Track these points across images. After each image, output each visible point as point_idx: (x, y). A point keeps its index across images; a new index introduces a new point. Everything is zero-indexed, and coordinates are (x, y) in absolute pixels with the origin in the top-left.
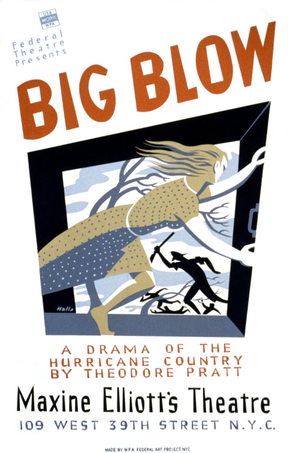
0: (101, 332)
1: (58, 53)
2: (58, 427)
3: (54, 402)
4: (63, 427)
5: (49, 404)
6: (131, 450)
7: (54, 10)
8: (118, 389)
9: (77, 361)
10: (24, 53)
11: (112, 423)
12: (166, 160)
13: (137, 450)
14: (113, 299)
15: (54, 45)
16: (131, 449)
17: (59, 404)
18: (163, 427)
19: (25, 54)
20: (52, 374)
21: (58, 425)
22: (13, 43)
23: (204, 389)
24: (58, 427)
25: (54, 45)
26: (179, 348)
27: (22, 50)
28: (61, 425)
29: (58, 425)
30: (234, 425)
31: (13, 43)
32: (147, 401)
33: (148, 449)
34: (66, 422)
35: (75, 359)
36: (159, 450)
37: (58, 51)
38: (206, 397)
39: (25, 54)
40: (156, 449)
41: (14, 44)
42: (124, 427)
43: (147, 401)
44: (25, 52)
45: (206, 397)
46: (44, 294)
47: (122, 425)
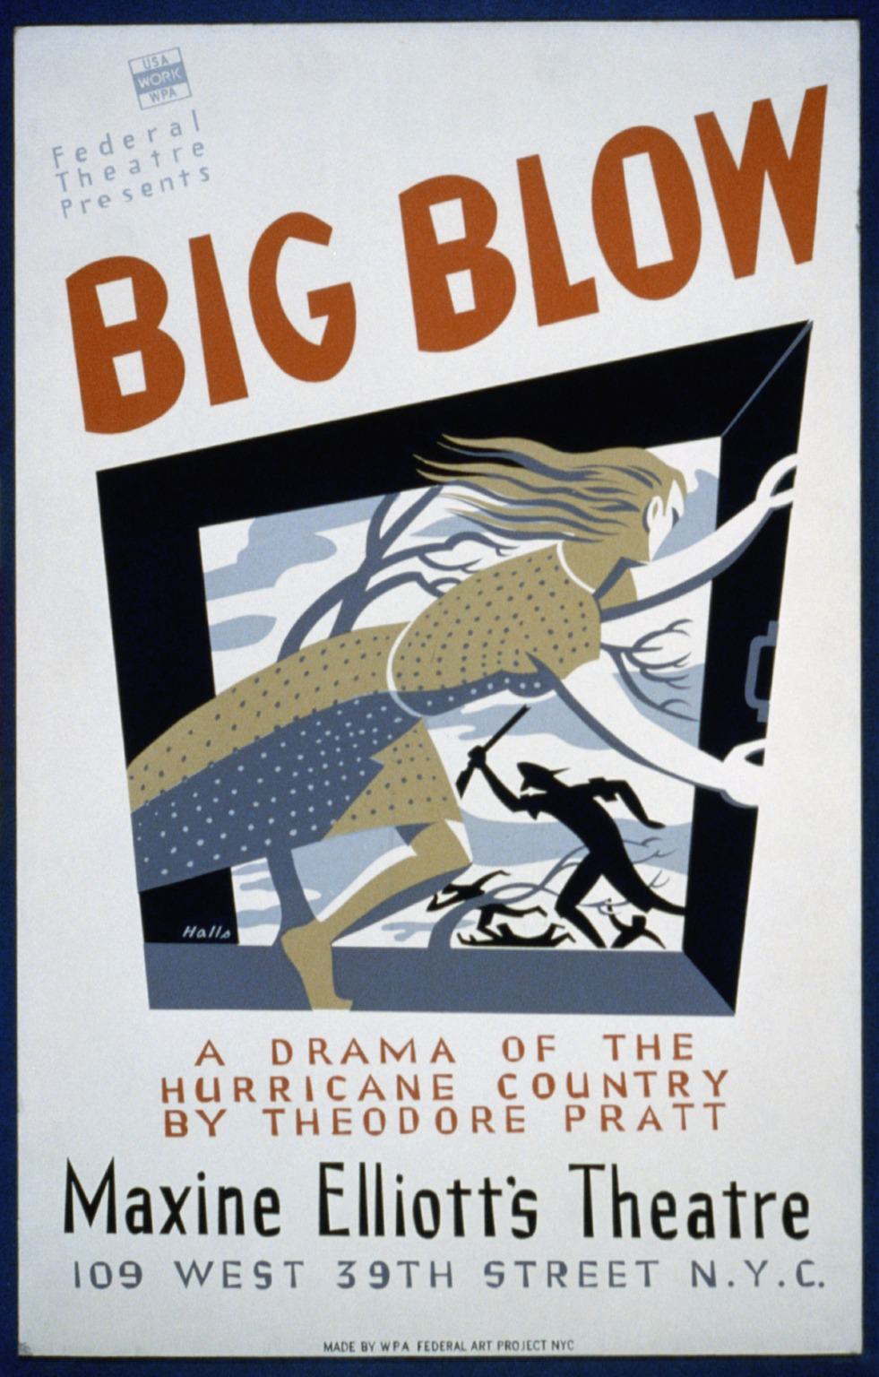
2: (186, 1281)
3: (175, 1207)
21: (186, 1273)
24: (186, 1281)
26: (541, 1048)
29: (186, 1273)
32: (447, 1203)
41: (58, 151)
43: (447, 1203)
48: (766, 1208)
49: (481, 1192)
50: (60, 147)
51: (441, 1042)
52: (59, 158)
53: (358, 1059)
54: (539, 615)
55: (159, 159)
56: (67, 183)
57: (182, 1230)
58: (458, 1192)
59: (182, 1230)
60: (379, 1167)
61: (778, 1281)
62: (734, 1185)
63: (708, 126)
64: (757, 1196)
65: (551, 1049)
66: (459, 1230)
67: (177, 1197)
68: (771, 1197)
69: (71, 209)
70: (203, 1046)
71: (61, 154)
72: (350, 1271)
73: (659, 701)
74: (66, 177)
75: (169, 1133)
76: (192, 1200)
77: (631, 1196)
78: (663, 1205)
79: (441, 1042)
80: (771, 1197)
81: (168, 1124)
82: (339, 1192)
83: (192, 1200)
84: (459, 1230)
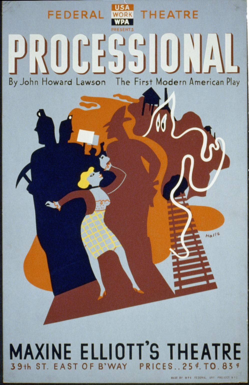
2: (110, 368)
3: (40, 350)
4: (114, 368)
5: (35, 352)
6: (189, 378)
8: (110, 345)
11: (114, 365)
12: (107, 152)
13: (195, 378)
16: (190, 377)
17: (44, 351)
18: (38, 368)
21: (110, 366)
23: (93, 345)
24: (110, 368)
28: (112, 366)
29: (110, 366)
33: (202, 377)
34: (115, 364)
36: (220, 377)
37: (150, 80)
40: (210, 377)
42: (20, 368)
46: (95, 281)
47: (18, 366)
49: (150, 81)
50: (57, 364)
52: (92, 367)
53: (192, 84)
56: (207, 367)
57: (37, 345)
59: (37, 345)
60: (140, 84)
61: (210, 78)
62: (151, 80)
63: (161, 84)
66: (30, 84)
67: (40, 347)
68: (66, 81)
69: (143, 367)
71: (93, 366)
73: (15, 84)
74: (77, 365)
75: (99, 369)
81: (99, 366)
84: (30, 84)
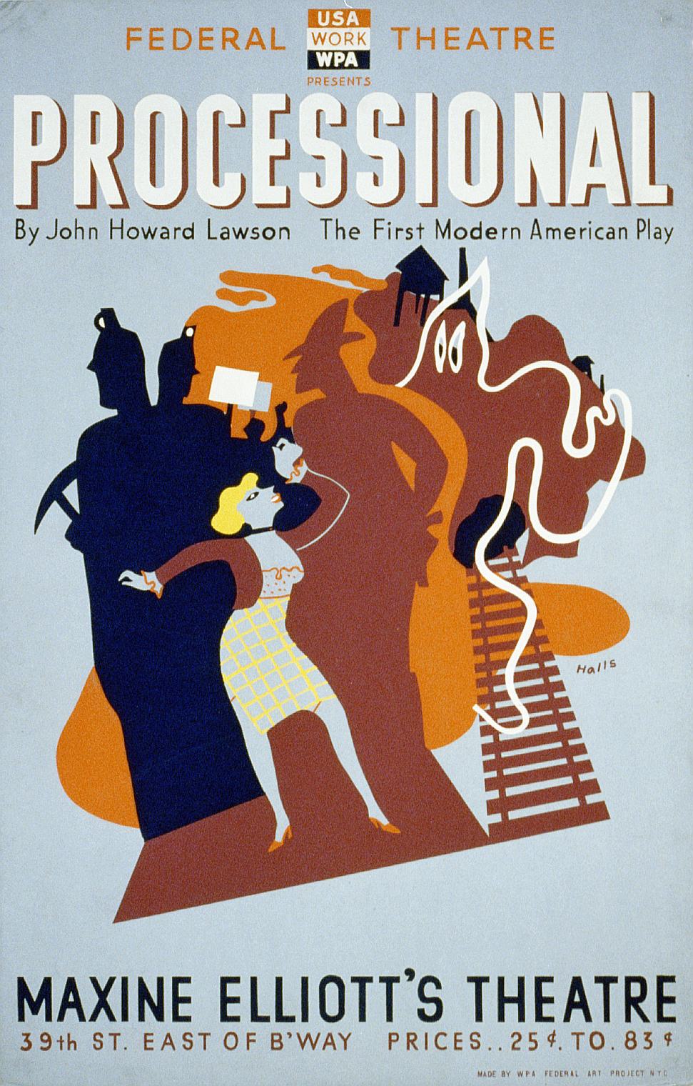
0: (379, 135)
1: (422, 231)
2: (303, 1045)
3: (103, 995)
7: (284, 201)
9: (277, 1045)
10: (72, 1045)
14: (526, 806)
15: (581, 234)
19: (75, 1048)
20: (273, 1041)
22: (146, 1035)
24: (303, 1045)
25: (581, 234)
26: (249, 1041)
27: (583, 1034)
30: (311, 1040)
31: (146, 1035)
32: (352, 991)
35: (273, 1035)
38: (71, 1040)
39: (75, 1048)
41: (149, 1038)
43: (352, 991)
44: (75, 1042)
45: (71, 1040)
48: (583, 233)
51: (168, 1035)
54: (495, 1049)
55: (670, 1043)
58: (504, 230)
64: (193, 238)
65: (254, 1041)
70: (143, 1044)
72: (650, 1038)
76: (117, 985)
77: (342, 228)
78: (658, 235)
79: (168, 1035)
80: (179, 229)
82: (550, 1000)
83: (117, 985)
